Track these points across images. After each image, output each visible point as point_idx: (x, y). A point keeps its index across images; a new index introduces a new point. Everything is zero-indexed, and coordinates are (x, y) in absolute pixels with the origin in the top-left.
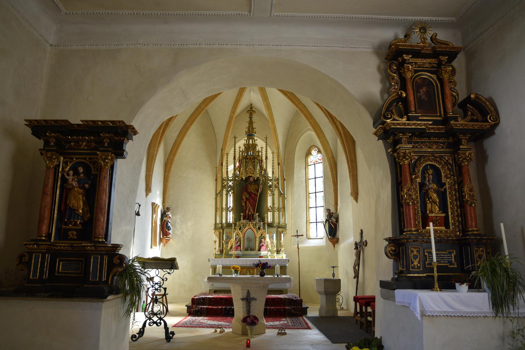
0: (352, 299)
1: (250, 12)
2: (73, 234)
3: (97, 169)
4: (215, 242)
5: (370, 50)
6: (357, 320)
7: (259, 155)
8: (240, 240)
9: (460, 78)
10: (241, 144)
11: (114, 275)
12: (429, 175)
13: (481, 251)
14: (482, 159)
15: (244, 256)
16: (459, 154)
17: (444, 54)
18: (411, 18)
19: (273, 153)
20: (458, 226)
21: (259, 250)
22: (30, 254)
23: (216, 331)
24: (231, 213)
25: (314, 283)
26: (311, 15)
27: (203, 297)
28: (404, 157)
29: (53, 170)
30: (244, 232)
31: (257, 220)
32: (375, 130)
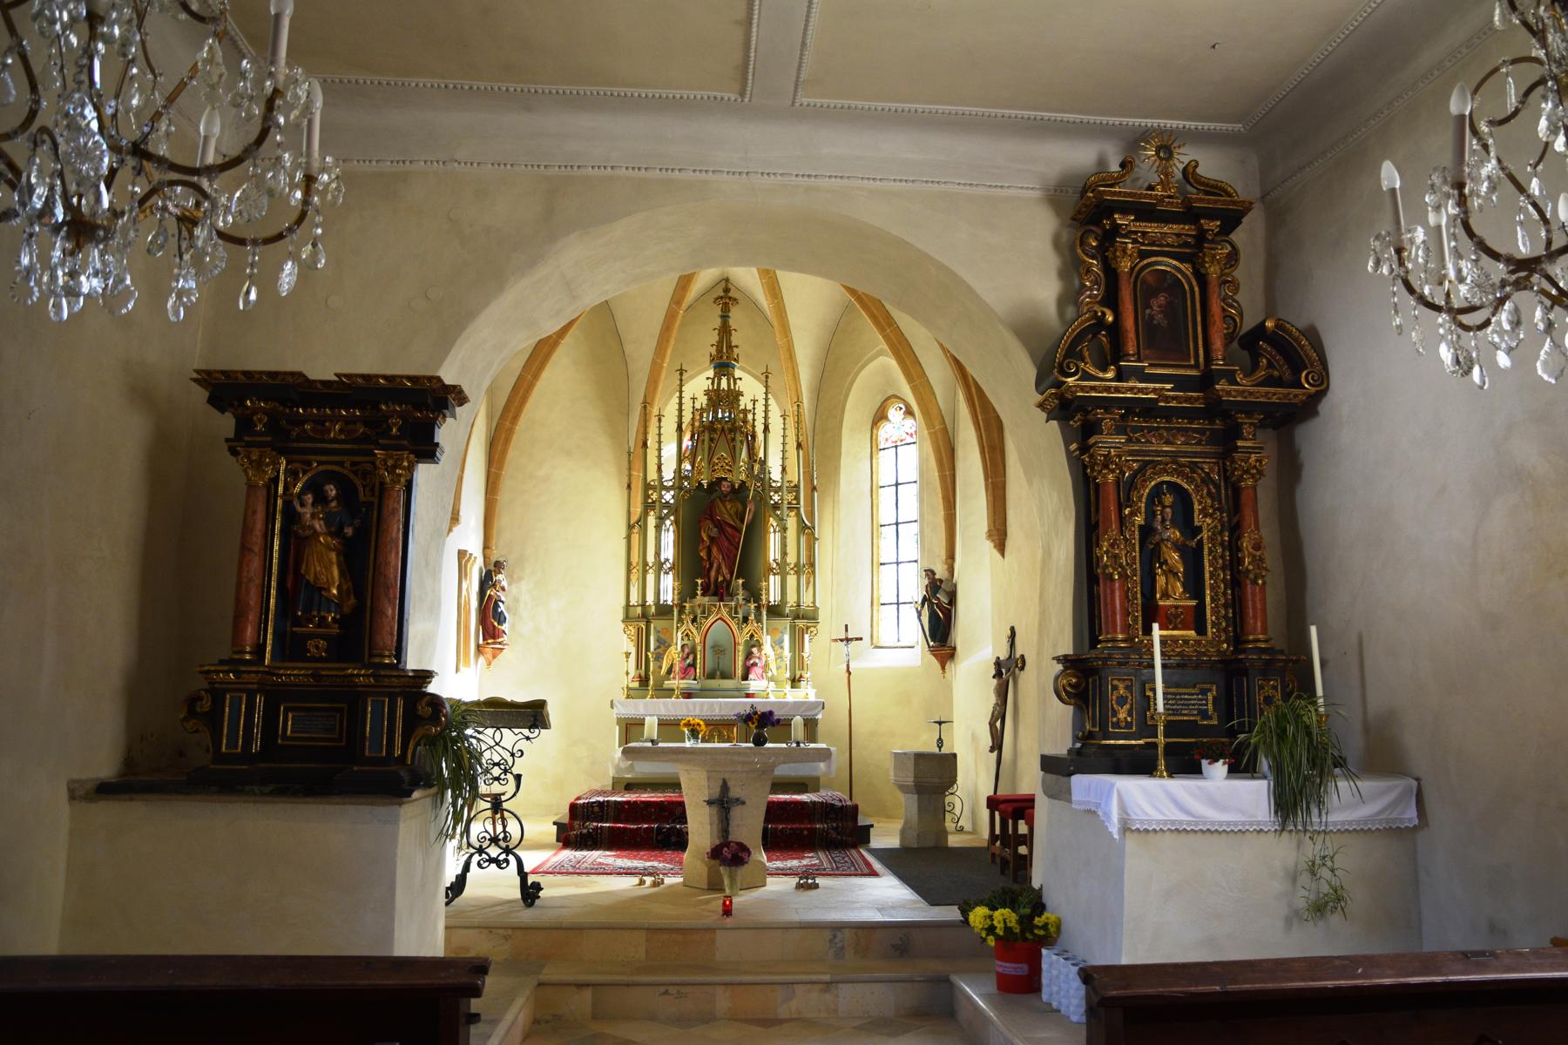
0: (984, 803)
1: (742, 94)
2: (317, 647)
3: (372, 490)
4: (628, 655)
5: (1037, 194)
6: (993, 855)
7: (745, 421)
8: (693, 651)
9: (1250, 273)
10: (698, 386)
11: (418, 744)
12: (1164, 507)
13: (1272, 688)
14: (1290, 469)
15: (704, 693)
16: (1233, 461)
17: (1211, 214)
18: (1137, 121)
19: (784, 417)
20: (1225, 630)
21: (745, 678)
22: (217, 694)
23: (642, 882)
24: (671, 576)
25: (889, 764)
26: (893, 105)
27: (601, 799)
28: (1106, 466)
29: (264, 493)
30: (704, 628)
31: (740, 597)
32: (1040, 398)
